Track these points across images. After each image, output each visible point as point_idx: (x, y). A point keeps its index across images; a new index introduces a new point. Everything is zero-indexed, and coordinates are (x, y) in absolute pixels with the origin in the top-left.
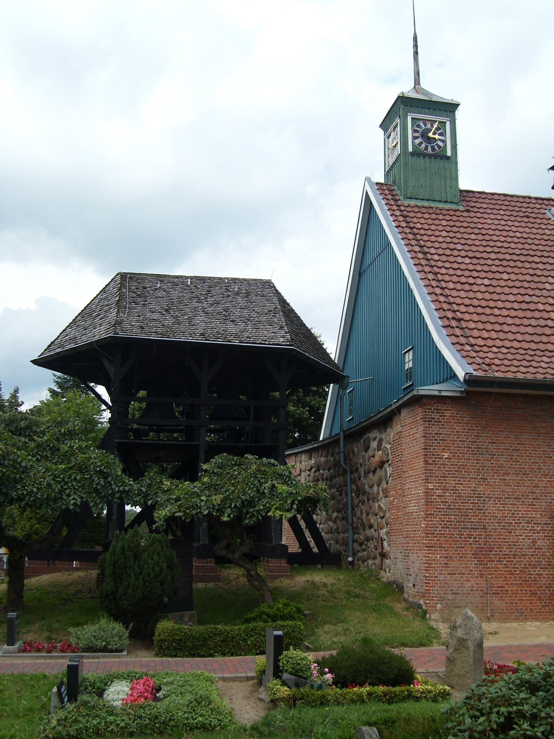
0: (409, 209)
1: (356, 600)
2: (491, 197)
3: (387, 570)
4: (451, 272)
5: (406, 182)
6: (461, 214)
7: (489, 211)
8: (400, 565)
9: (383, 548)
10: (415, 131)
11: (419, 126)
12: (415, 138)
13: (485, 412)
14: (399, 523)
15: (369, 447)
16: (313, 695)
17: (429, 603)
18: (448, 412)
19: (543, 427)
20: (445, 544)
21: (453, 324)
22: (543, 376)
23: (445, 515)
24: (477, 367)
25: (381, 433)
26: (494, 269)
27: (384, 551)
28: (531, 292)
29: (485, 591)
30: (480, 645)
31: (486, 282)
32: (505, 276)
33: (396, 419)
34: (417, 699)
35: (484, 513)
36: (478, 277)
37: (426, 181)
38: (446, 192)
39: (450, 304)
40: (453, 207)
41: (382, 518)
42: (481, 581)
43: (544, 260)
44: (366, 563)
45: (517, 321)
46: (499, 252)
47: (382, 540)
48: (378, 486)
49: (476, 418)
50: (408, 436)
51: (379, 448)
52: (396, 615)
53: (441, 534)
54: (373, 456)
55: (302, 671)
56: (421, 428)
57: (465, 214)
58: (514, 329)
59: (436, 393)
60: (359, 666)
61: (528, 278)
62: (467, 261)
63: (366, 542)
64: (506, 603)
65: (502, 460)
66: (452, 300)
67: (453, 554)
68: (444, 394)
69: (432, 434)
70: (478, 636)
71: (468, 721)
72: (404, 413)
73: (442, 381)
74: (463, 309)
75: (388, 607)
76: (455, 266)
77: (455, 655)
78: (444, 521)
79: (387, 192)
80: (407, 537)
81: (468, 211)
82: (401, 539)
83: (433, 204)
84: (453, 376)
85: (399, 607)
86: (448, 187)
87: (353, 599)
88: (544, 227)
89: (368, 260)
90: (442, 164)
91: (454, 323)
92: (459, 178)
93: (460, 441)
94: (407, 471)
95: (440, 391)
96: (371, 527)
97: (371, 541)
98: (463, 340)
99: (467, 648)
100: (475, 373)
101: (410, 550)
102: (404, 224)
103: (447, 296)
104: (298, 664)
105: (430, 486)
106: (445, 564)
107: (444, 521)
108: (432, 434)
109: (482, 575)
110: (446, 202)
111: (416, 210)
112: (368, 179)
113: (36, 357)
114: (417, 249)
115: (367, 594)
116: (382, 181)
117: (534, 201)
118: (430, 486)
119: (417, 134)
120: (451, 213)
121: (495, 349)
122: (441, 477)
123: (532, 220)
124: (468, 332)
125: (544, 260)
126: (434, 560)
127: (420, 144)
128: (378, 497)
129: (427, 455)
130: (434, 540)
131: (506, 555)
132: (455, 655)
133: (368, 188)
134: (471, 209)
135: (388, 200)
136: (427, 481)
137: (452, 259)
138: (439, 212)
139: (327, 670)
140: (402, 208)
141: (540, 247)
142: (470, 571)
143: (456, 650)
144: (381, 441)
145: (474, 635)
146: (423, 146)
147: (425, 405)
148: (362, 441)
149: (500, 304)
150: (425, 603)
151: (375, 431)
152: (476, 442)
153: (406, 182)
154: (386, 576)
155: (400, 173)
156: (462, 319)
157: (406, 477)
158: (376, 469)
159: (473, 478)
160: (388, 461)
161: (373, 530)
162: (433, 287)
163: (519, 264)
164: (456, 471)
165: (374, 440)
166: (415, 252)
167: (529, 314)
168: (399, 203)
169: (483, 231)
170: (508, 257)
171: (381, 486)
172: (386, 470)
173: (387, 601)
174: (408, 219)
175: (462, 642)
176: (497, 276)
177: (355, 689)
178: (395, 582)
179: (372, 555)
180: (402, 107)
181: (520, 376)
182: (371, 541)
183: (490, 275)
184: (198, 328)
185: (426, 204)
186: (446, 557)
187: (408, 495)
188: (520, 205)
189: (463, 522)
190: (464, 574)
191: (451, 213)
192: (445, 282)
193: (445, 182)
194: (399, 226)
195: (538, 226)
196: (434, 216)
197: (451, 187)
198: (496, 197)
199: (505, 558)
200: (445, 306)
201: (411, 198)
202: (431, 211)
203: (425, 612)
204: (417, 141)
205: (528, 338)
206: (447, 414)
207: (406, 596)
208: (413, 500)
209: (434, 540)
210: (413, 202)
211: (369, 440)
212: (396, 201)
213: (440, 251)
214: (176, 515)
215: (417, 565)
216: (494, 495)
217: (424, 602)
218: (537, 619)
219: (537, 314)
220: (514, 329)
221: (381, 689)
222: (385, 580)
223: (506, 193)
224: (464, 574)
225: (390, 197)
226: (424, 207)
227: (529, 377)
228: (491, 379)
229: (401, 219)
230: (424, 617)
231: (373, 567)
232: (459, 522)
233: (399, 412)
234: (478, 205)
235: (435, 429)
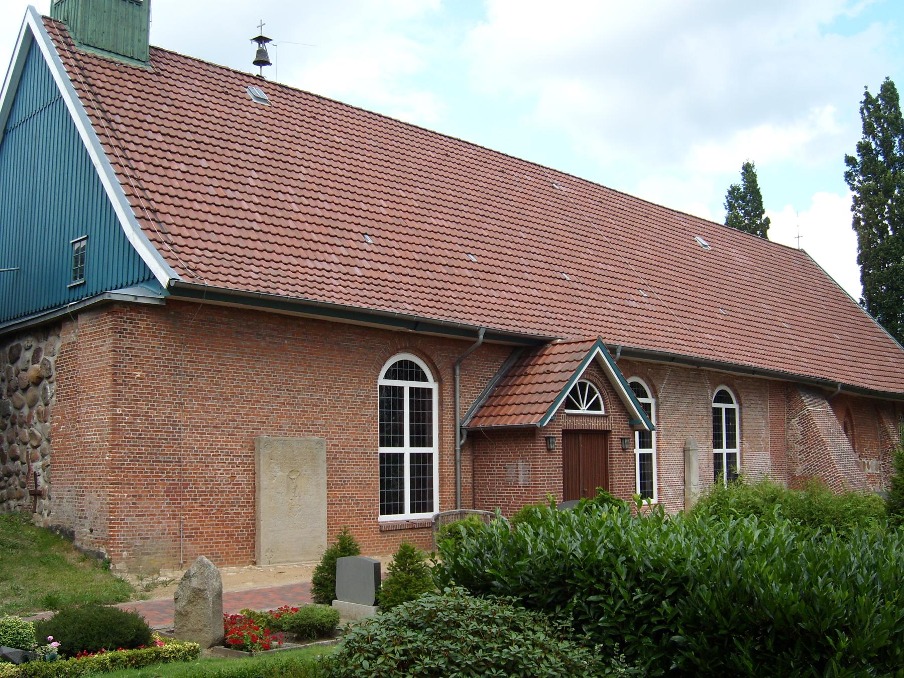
0: (87, 60)
1: (14, 551)
2: (184, 61)
3: (45, 513)
4: (141, 149)
5: (84, 23)
6: (149, 76)
7: (182, 78)
8: (67, 507)
9: (36, 486)
13: (185, 326)
14: (68, 455)
15: (18, 358)
16: (48, 668)
17: (114, 551)
18: (144, 323)
19: (248, 347)
20: (134, 480)
21: (148, 216)
22: (265, 290)
23: (134, 446)
24: (182, 272)
25: (39, 341)
26: (191, 152)
27: (39, 489)
28: (233, 186)
29: (178, 535)
30: (219, 595)
31: (183, 167)
32: (204, 163)
33: (68, 326)
34: (166, 660)
35: (179, 444)
36: (173, 160)
37: (109, 27)
38: (133, 46)
39: (143, 189)
40: (140, 66)
41: (35, 447)
42: (173, 522)
43: (247, 149)
44: (5, 505)
45: (220, 220)
46: (197, 132)
47: (36, 475)
48: (31, 407)
49: (175, 332)
50: (89, 348)
51: (35, 359)
52: (70, 567)
53: (130, 468)
54: (26, 370)
55: (23, 641)
56: (109, 341)
57: (155, 78)
58: (217, 229)
59: (131, 299)
60: (90, 629)
61: (229, 168)
62: (160, 138)
63: (6, 478)
64: (201, 547)
65: (202, 382)
66: (145, 185)
67: (143, 492)
68: (140, 301)
69: (122, 348)
70: (216, 584)
71: (366, 664)
72: (83, 320)
73: (130, 283)
74: (158, 198)
75: (58, 558)
76: (146, 142)
77: (189, 608)
78: (133, 453)
79: (57, 32)
80: (81, 472)
81: (158, 74)
82: (69, 474)
83: (116, 59)
84: (150, 278)
85: (72, 557)
86: (136, 40)
87: (10, 551)
88: (245, 109)
89: (20, 114)
90: (130, 9)
91: (149, 215)
92: (151, 31)
93: (155, 358)
94: (84, 392)
95: (136, 297)
96: (15, 458)
97: (14, 477)
98: (161, 237)
99: (204, 599)
100: (181, 279)
101: (86, 487)
102: (81, 79)
103: (138, 180)
104: (19, 634)
105: (119, 411)
106: (134, 504)
107: (133, 453)
108: (122, 348)
109: (174, 516)
110: (132, 58)
111: (95, 62)
112: (31, 9)
114: (99, 113)
115: (26, 543)
116: (48, 15)
117: (233, 75)
118: (119, 411)
120: (139, 74)
121: (197, 252)
122: (132, 400)
123: (232, 98)
124: (166, 228)
125: (247, 149)
126: (120, 500)
128: (29, 421)
129: (116, 373)
130: (120, 476)
131: (202, 492)
132: (189, 608)
133: (31, 20)
134: (162, 73)
135: (58, 42)
136: (115, 404)
137: (141, 133)
138: (123, 69)
139: (51, 637)
140: (78, 57)
141: (242, 133)
142: (162, 511)
143: (190, 602)
144: (38, 352)
145: (212, 584)
147: (116, 312)
148: (7, 349)
149: (199, 197)
150: (109, 552)
151: (30, 339)
152: (173, 360)
153: (84, 23)
154: (43, 520)
155: (76, 10)
156: (158, 211)
157: (82, 399)
158: (28, 386)
159: (169, 403)
160: (49, 377)
161: (19, 462)
162: (121, 166)
163: (218, 150)
164: (149, 394)
165: (26, 350)
166: (97, 118)
167: (232, 213)
168: (74, 49)
169: (177, 104)
170: (207, 140)
171: (36, 407)
172: (45, 388)
173: (54, 549)
174: (86, 73)
175: (198, 593)
176: (195, 161)
177: (96, 656)
178: (57, 527)
179: (16, 494)
181: (231, 287)
182: (14, 477)
183: (187, 160)
185: (107, 56)
186: (134, 496)
187: (84, 421)
188: (218, 77)
189: (156, 454)
190: (155, 515)
191: (139, 74)
192: (135, 161)
193: (133, 33)
194: (75, 80)
195: (238, 107)
196: (117, 74)
197: (139, 41)
198: (190, 62)
199: (200, 496)
200: (138, 192)
201: (88, 45)
202: (113, 67)
203: (109, 562)
205: (233, 241)
206: (142, 325)
207: (78, 544)
208: (92, 427)
209: (120, 476)
210: (90, 51)
211: (19, 348)
212: (69, 45)
213: (127, 121)
215: (97, 506)
216: (191, 422)
217: (107, 551)
218: (233, 564)
219: (241, 214)
220: (217, 229)
221: (124, 653)
222: (42, 525)
223: (202, 59)
224: (155, 515)
225: (61, 38)
226: (104, 60)
227: (242, 288)
228: (201, 288)
229: (77, 70)
230: (106, 568)
231: (18, 509)
232: (151, 454)
233: (76, 318)
234: (170, 69)
235: (127, 342)
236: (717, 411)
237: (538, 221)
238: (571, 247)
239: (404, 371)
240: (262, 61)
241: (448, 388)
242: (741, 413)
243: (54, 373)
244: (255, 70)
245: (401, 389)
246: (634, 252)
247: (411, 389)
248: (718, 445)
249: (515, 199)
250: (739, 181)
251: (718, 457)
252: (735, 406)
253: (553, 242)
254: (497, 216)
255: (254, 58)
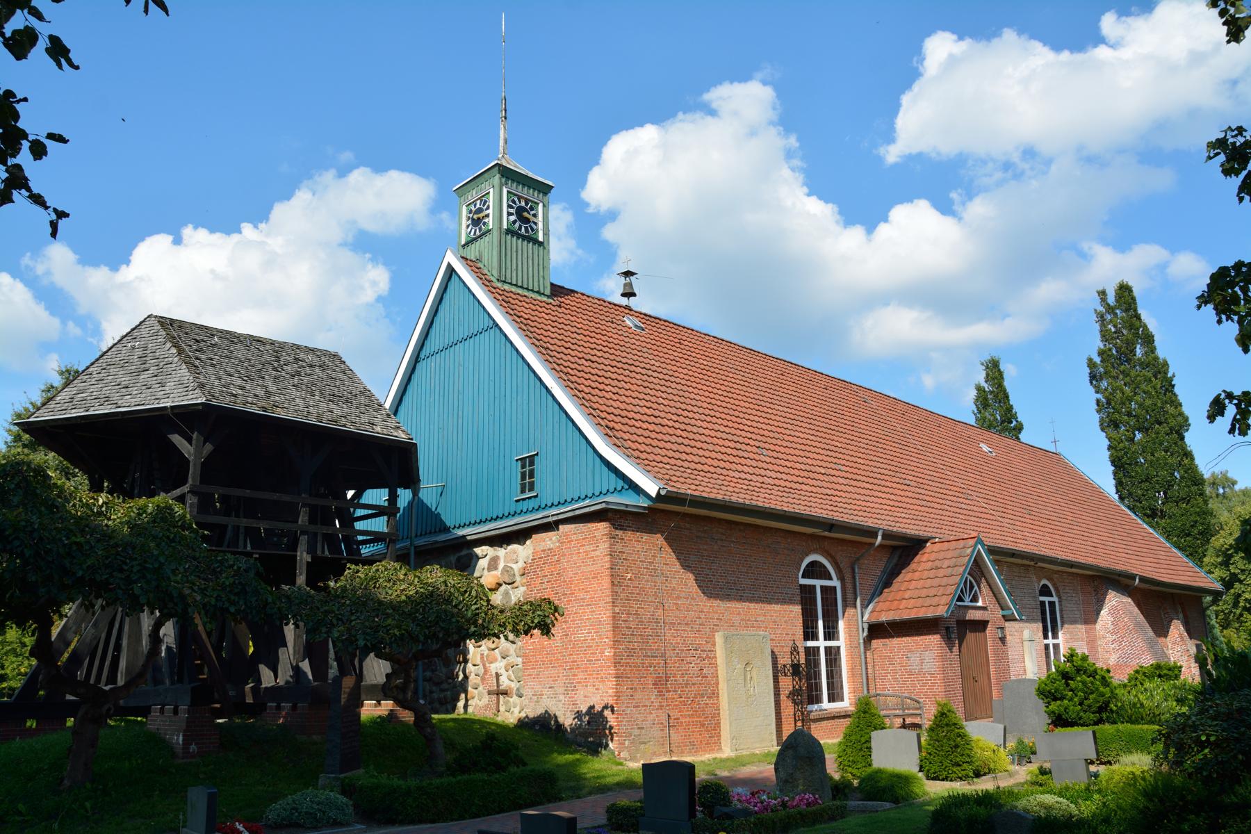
10: (509, 206)
11: (514, 202)
12: (509, 214)
65: (674, 582)
95: (627, 506)
105: (617, 609)
118: (617, 609)
119: (511, 211)
127: (514, 222)
146: (517, 225)
184: (295, 405)
204: (513, 218)
235: (619, 547)
236: (1043, 603)
237: (699, 404)
238: (738, 432)
239: (815, 570)
240: (629, 294)
241: (849, 586)
243: (518, 579)
247: (822, 587)
248: (1046, 637)
249: (700, 386)
250: (980, 377)
252: (1055, 599)
253: (727, 430)
255: (621, 291)
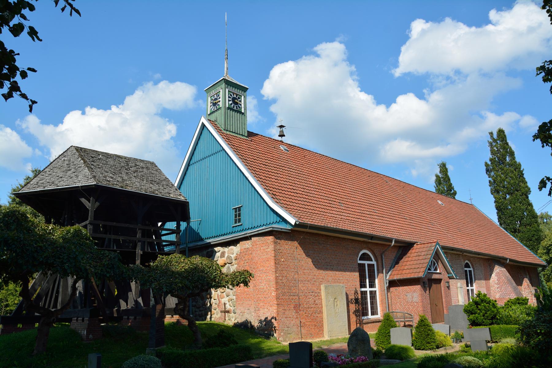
10: (229, 97)
11: (231, 95)
12: (229, 101)
113: (317, 59)
119: (230, 99)
127: (231, 104)
146: (232, 105)
180: (224, 84)
204: (231, 102)
214: (209, 313)
235: (278, 247)
236: (466, 271)
240: (282, 135)
242: (474, 272)
243: (234, 261)
244: (280, 139)
245: (365, 264)
246: (269, 173)
248: (468, 286)
250: (437, 171)
251: (468, 290)
254: (319, 180)
255: (278, 134)
